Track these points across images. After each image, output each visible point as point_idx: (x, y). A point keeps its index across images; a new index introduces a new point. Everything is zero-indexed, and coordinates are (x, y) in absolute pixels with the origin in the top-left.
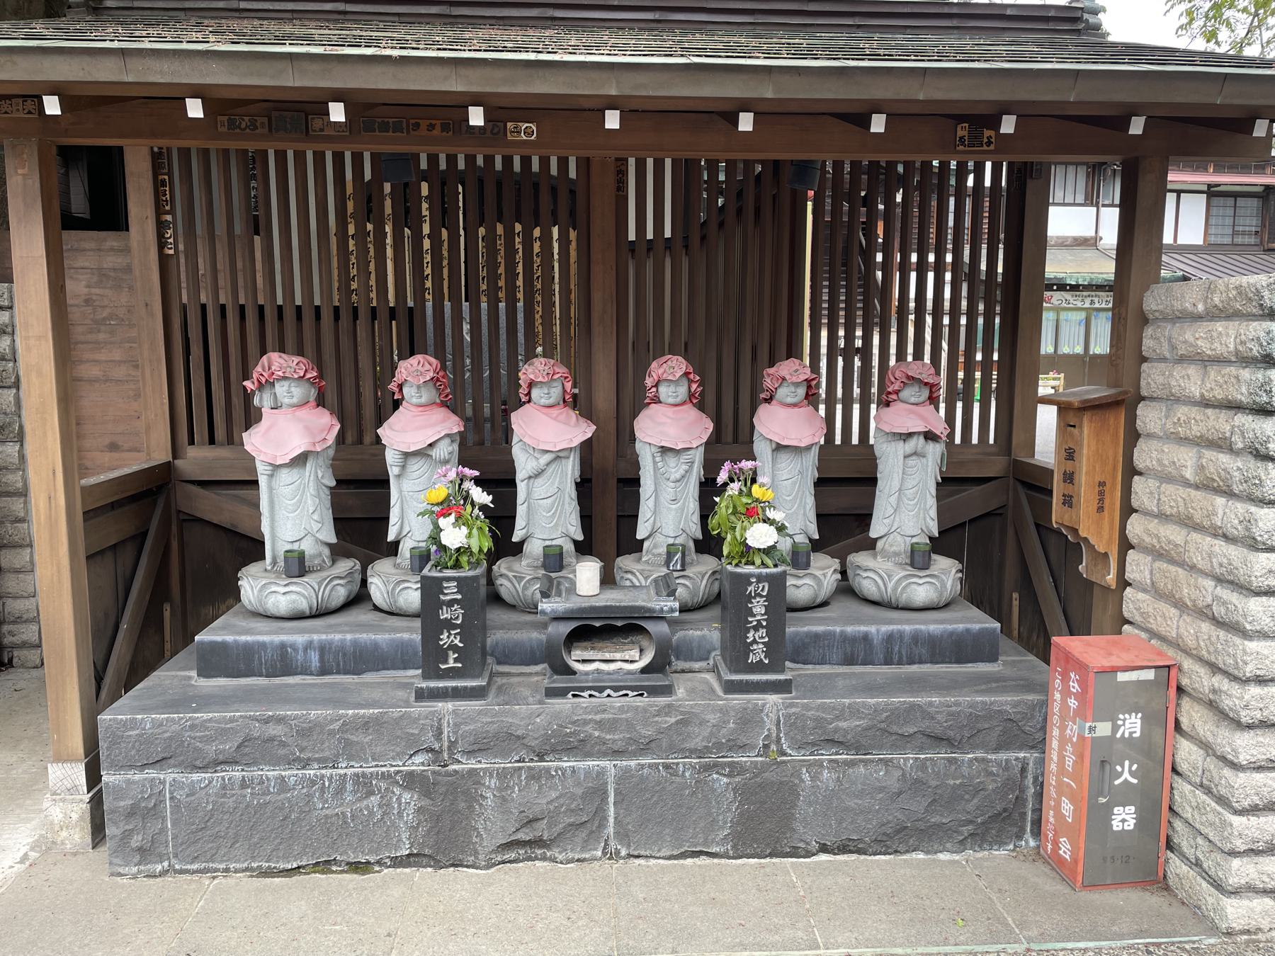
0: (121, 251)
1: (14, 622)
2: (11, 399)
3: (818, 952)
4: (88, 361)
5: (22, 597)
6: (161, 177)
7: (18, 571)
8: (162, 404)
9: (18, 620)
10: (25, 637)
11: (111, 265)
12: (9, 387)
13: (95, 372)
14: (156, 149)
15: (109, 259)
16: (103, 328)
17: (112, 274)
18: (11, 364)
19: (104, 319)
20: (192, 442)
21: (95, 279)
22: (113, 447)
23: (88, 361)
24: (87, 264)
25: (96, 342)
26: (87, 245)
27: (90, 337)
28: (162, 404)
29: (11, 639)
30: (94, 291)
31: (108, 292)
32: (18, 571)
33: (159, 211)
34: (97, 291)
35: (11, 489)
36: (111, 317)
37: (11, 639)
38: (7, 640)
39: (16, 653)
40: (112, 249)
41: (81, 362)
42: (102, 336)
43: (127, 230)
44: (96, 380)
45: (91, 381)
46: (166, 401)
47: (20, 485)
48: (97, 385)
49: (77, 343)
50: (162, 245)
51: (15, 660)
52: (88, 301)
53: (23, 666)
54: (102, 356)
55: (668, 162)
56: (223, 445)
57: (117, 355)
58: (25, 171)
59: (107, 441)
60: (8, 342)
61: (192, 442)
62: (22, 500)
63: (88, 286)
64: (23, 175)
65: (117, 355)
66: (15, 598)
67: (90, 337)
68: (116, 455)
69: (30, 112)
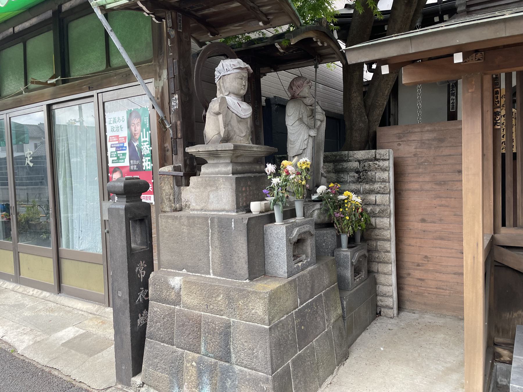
0: (432, 131)
1: (382, 296)
2: (388, 199)
3: (208, 276)
4: (413, 182)
5: (386, 285)
6: (495, 90)
7: (385, 274)
8: (490, 205)
9: (384, 295)
10: (387, 303)
11: (427, 138)
12: (387, 194)
13: (416, 186)
14: (494, 76)
15: (426, 135)
16: (421, 166)
17: (427, 142)
18: (388, 184)
19: (422, 163)
20: (504, 225)
21: (419, 145)
22: (423, 221)
23: (413, 182)
24: (416, 138)
25: (418, 173)
26: (416, 130)
27: (415, 171)
28: (490, 205)
29: (381, 303)
30: (418, 150)
31: (425, 150)
32: (385, 274)
33: (494, 106)
34: (420, 150)
35: (385, 238)
36: (425, 162)
37: (381, 303)
38: (379, 303)
39: (382, 310)
40: (428, 131)
41: (411, 182)
42: (420, 170)
43: (448, 120)
44: (417, 190)
45: (415, 190)
46: (492, 204)
47: (389, 236)
48: (417, 192)
49: (409, 174)
50: (495, 123)
51: (382, 313)
52: (415, 155)
53: (385, 316)
54: (420, 180)
55: (514, 74)
56: (510, 227)
57: (427, 179)
58: (473, 90)
59: (420, 217)
60: (387, 174)
61: (504, 225)
62: (389, 243)
63: (416, 148)
64: (472, 92)
65: (427, 179)
66: (383, 285)
67: (415, 171)
68: (424, 224)
69: (479, 60)
